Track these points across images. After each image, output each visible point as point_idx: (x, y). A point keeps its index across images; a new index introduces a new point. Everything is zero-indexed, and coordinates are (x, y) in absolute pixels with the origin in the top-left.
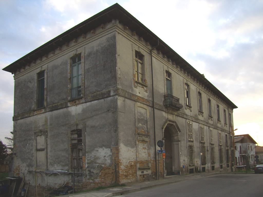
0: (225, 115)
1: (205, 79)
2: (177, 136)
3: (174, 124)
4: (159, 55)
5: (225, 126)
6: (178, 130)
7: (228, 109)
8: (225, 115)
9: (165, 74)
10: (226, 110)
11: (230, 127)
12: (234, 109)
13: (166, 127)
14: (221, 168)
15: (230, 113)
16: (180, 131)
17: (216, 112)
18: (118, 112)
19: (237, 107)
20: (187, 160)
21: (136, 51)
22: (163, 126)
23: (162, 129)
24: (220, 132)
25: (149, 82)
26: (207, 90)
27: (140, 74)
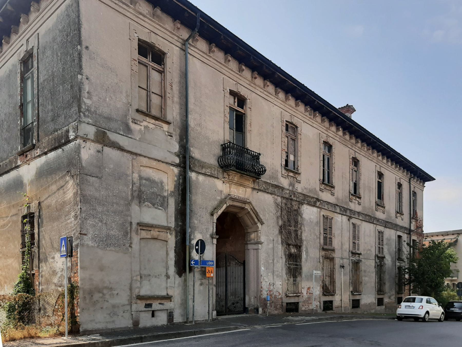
0: (400, 195)
1: (241, 42)
2: (256, 233)
3: (247, 207)
4: (211, 55)
5: (396, 217)
6: (256, 220)
7: (410, 183)
8: (400, 195)
9: (322, 146)
10: (405, 185)
11: (413, 221)
12: (426, 183)
13: (223, 213)
14: (378, 305)
15: (415, 191)
16: (262, 223)
17: (374, 186)
18: (449, 251)
19: (435, 179)
20: (281, 283)
21: (378, 172)
22: (216, 208)
23: (212, 215)
24: (381, 228)
25: (173, 112)
26: (396, 167)
27: (153, 96)
